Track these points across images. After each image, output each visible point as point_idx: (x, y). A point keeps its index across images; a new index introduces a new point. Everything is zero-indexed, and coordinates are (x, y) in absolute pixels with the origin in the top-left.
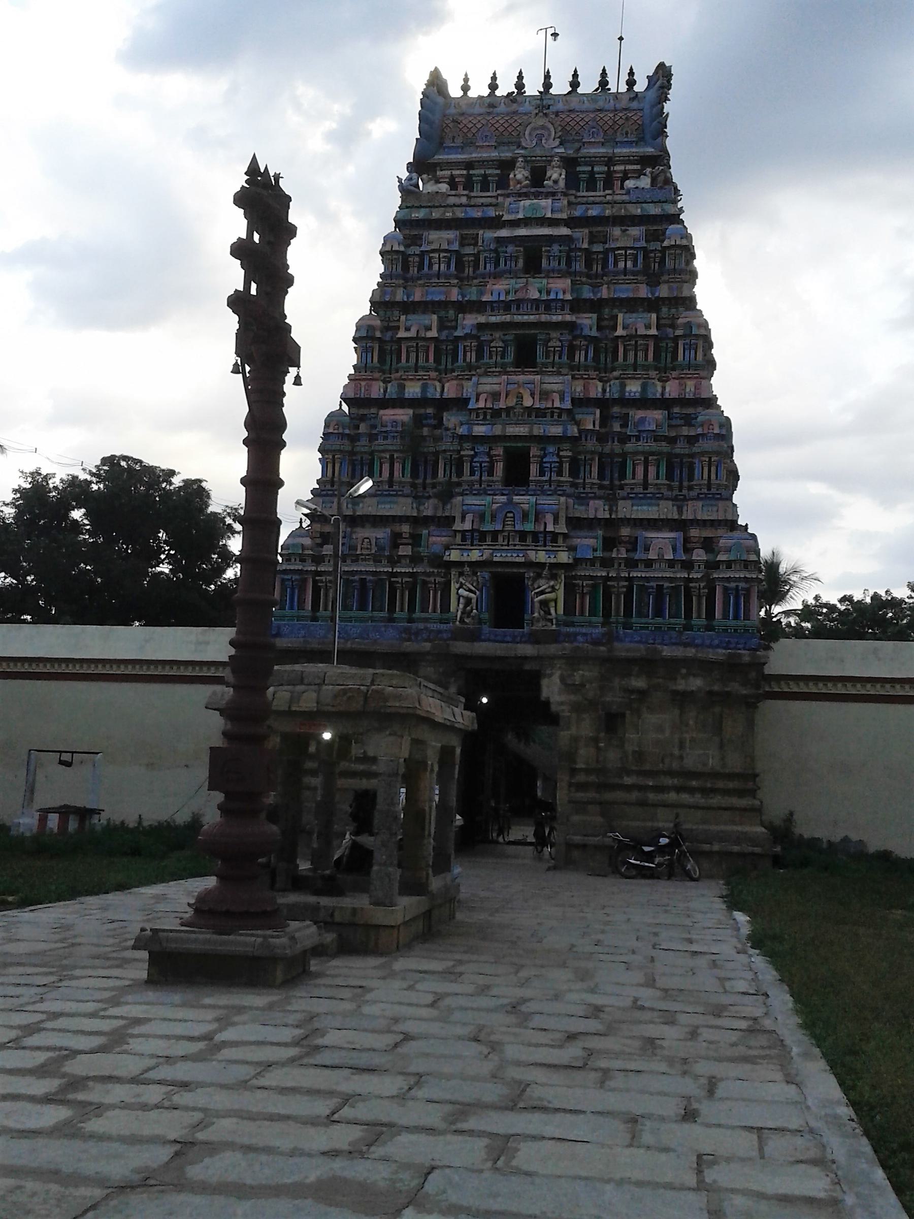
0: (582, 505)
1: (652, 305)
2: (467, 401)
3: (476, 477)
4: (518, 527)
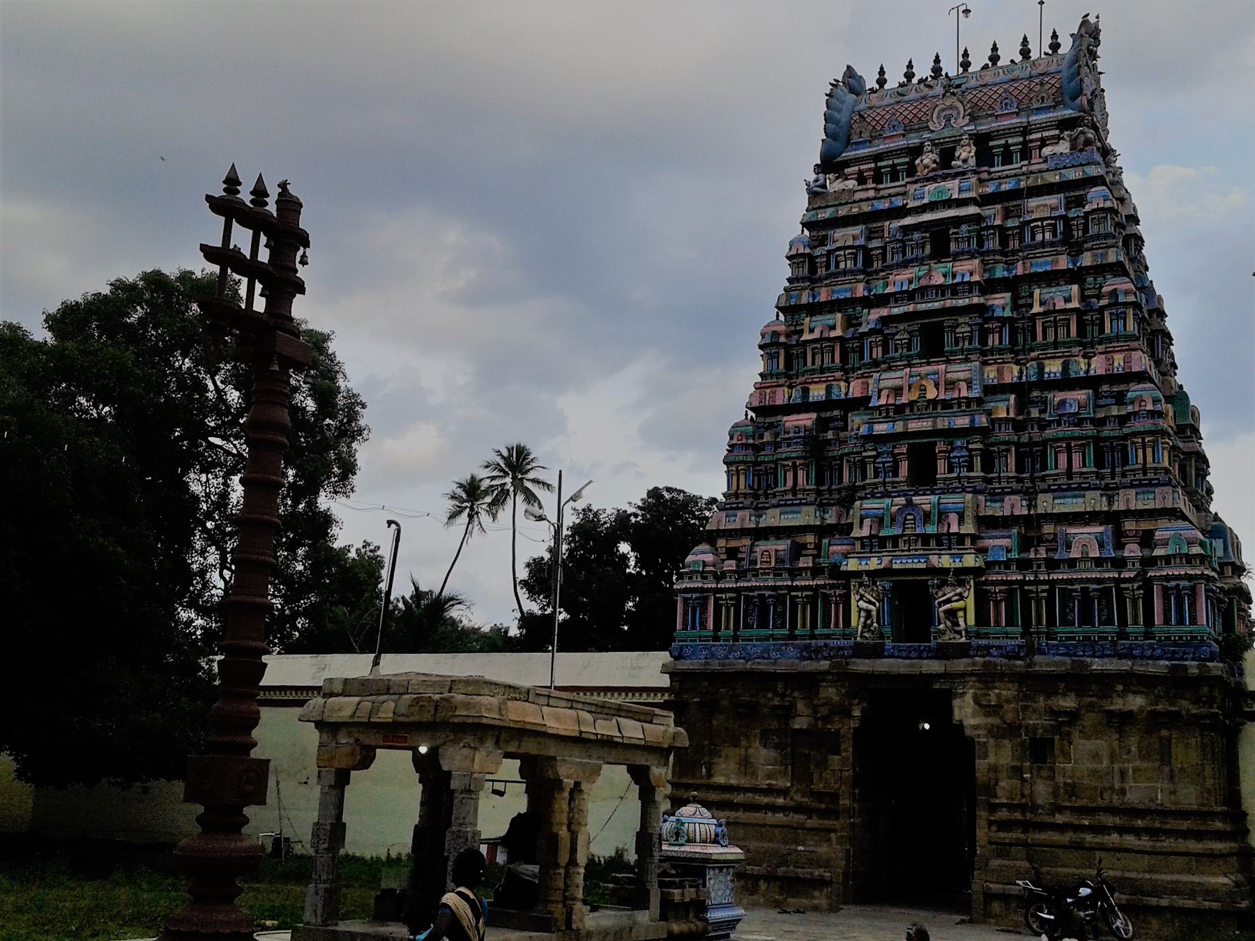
0: (996, 501)
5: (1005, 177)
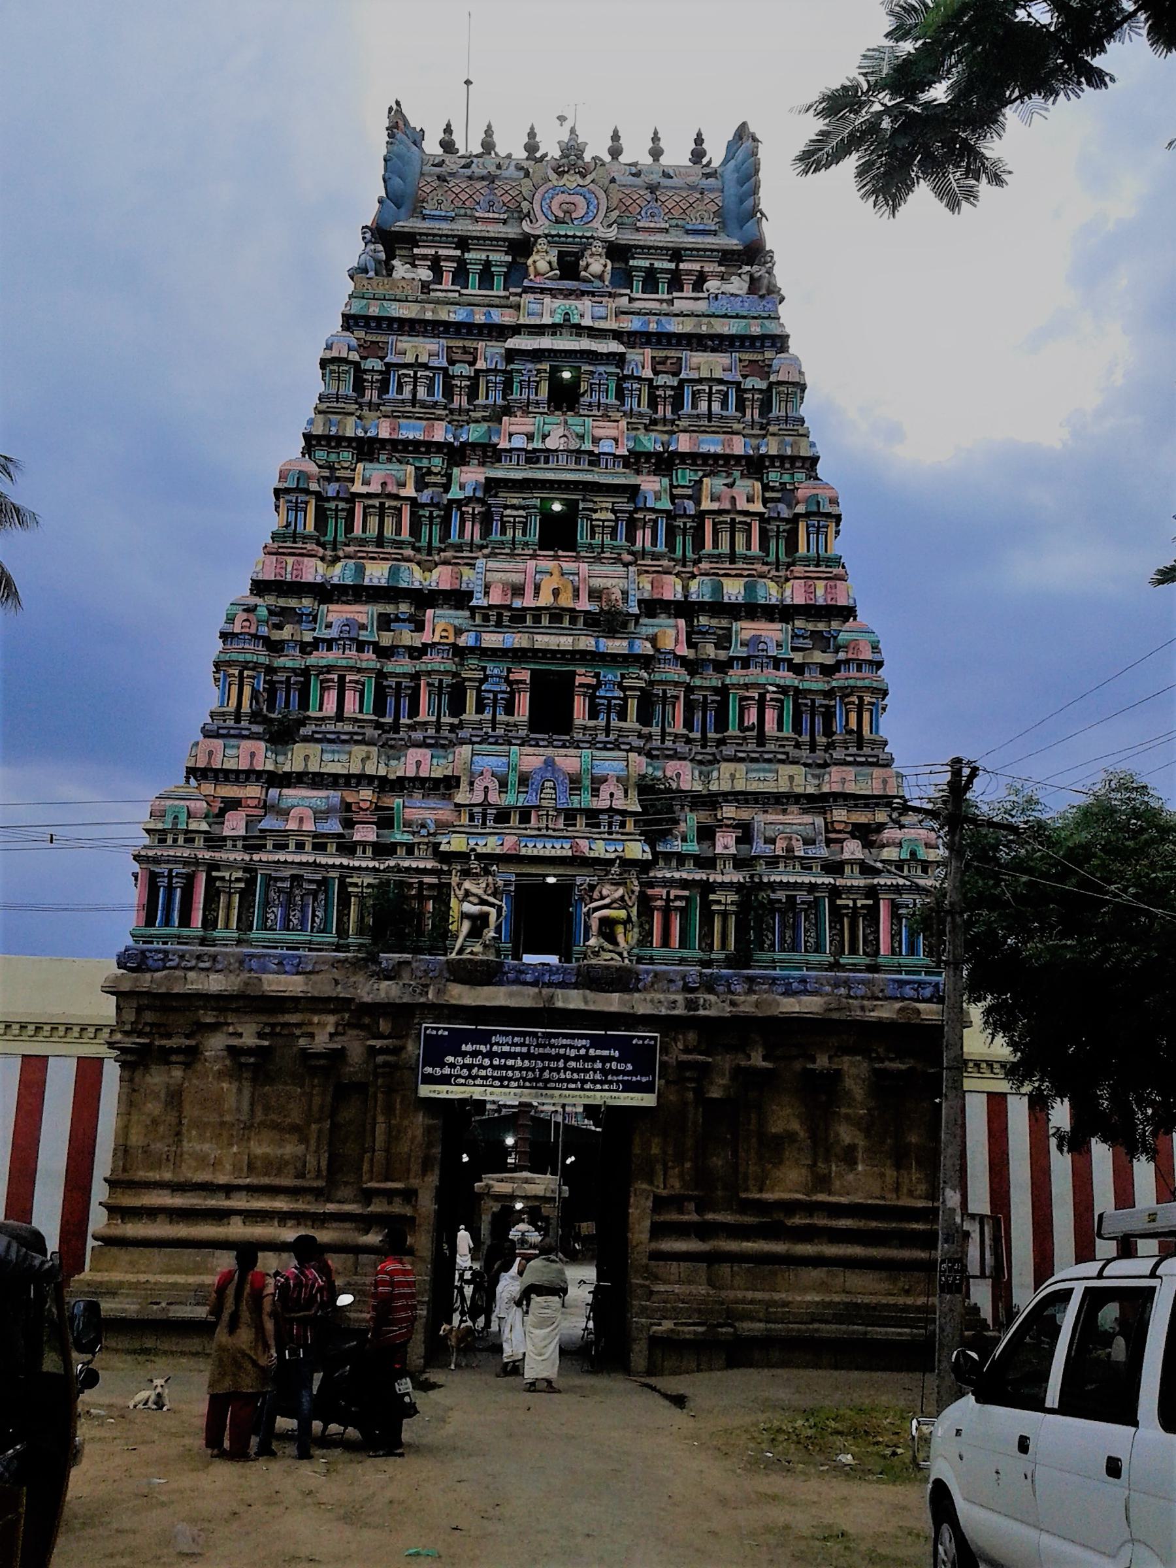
1: (755, 466)
2: (470, 595)
3: (487, 715)
4: (563, 803)
5: (643, 309)
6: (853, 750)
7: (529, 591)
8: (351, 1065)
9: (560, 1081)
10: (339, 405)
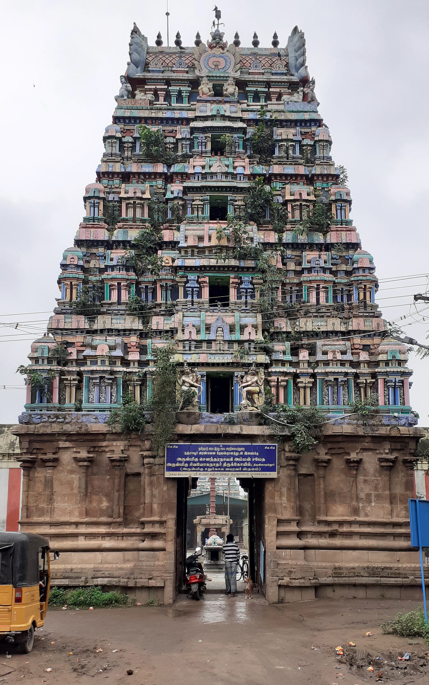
1: (310, 180)
6: (362, 310)
7: (206, 239)
8: (132, 464)
9: (231, 467)
10: (113, 158)
